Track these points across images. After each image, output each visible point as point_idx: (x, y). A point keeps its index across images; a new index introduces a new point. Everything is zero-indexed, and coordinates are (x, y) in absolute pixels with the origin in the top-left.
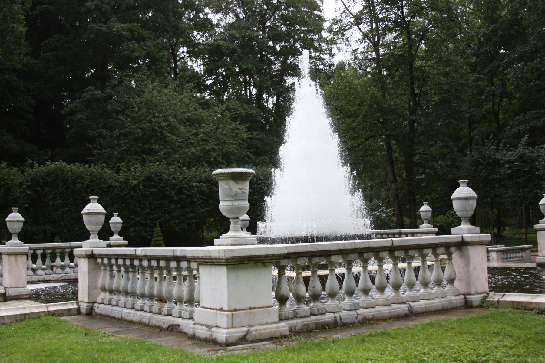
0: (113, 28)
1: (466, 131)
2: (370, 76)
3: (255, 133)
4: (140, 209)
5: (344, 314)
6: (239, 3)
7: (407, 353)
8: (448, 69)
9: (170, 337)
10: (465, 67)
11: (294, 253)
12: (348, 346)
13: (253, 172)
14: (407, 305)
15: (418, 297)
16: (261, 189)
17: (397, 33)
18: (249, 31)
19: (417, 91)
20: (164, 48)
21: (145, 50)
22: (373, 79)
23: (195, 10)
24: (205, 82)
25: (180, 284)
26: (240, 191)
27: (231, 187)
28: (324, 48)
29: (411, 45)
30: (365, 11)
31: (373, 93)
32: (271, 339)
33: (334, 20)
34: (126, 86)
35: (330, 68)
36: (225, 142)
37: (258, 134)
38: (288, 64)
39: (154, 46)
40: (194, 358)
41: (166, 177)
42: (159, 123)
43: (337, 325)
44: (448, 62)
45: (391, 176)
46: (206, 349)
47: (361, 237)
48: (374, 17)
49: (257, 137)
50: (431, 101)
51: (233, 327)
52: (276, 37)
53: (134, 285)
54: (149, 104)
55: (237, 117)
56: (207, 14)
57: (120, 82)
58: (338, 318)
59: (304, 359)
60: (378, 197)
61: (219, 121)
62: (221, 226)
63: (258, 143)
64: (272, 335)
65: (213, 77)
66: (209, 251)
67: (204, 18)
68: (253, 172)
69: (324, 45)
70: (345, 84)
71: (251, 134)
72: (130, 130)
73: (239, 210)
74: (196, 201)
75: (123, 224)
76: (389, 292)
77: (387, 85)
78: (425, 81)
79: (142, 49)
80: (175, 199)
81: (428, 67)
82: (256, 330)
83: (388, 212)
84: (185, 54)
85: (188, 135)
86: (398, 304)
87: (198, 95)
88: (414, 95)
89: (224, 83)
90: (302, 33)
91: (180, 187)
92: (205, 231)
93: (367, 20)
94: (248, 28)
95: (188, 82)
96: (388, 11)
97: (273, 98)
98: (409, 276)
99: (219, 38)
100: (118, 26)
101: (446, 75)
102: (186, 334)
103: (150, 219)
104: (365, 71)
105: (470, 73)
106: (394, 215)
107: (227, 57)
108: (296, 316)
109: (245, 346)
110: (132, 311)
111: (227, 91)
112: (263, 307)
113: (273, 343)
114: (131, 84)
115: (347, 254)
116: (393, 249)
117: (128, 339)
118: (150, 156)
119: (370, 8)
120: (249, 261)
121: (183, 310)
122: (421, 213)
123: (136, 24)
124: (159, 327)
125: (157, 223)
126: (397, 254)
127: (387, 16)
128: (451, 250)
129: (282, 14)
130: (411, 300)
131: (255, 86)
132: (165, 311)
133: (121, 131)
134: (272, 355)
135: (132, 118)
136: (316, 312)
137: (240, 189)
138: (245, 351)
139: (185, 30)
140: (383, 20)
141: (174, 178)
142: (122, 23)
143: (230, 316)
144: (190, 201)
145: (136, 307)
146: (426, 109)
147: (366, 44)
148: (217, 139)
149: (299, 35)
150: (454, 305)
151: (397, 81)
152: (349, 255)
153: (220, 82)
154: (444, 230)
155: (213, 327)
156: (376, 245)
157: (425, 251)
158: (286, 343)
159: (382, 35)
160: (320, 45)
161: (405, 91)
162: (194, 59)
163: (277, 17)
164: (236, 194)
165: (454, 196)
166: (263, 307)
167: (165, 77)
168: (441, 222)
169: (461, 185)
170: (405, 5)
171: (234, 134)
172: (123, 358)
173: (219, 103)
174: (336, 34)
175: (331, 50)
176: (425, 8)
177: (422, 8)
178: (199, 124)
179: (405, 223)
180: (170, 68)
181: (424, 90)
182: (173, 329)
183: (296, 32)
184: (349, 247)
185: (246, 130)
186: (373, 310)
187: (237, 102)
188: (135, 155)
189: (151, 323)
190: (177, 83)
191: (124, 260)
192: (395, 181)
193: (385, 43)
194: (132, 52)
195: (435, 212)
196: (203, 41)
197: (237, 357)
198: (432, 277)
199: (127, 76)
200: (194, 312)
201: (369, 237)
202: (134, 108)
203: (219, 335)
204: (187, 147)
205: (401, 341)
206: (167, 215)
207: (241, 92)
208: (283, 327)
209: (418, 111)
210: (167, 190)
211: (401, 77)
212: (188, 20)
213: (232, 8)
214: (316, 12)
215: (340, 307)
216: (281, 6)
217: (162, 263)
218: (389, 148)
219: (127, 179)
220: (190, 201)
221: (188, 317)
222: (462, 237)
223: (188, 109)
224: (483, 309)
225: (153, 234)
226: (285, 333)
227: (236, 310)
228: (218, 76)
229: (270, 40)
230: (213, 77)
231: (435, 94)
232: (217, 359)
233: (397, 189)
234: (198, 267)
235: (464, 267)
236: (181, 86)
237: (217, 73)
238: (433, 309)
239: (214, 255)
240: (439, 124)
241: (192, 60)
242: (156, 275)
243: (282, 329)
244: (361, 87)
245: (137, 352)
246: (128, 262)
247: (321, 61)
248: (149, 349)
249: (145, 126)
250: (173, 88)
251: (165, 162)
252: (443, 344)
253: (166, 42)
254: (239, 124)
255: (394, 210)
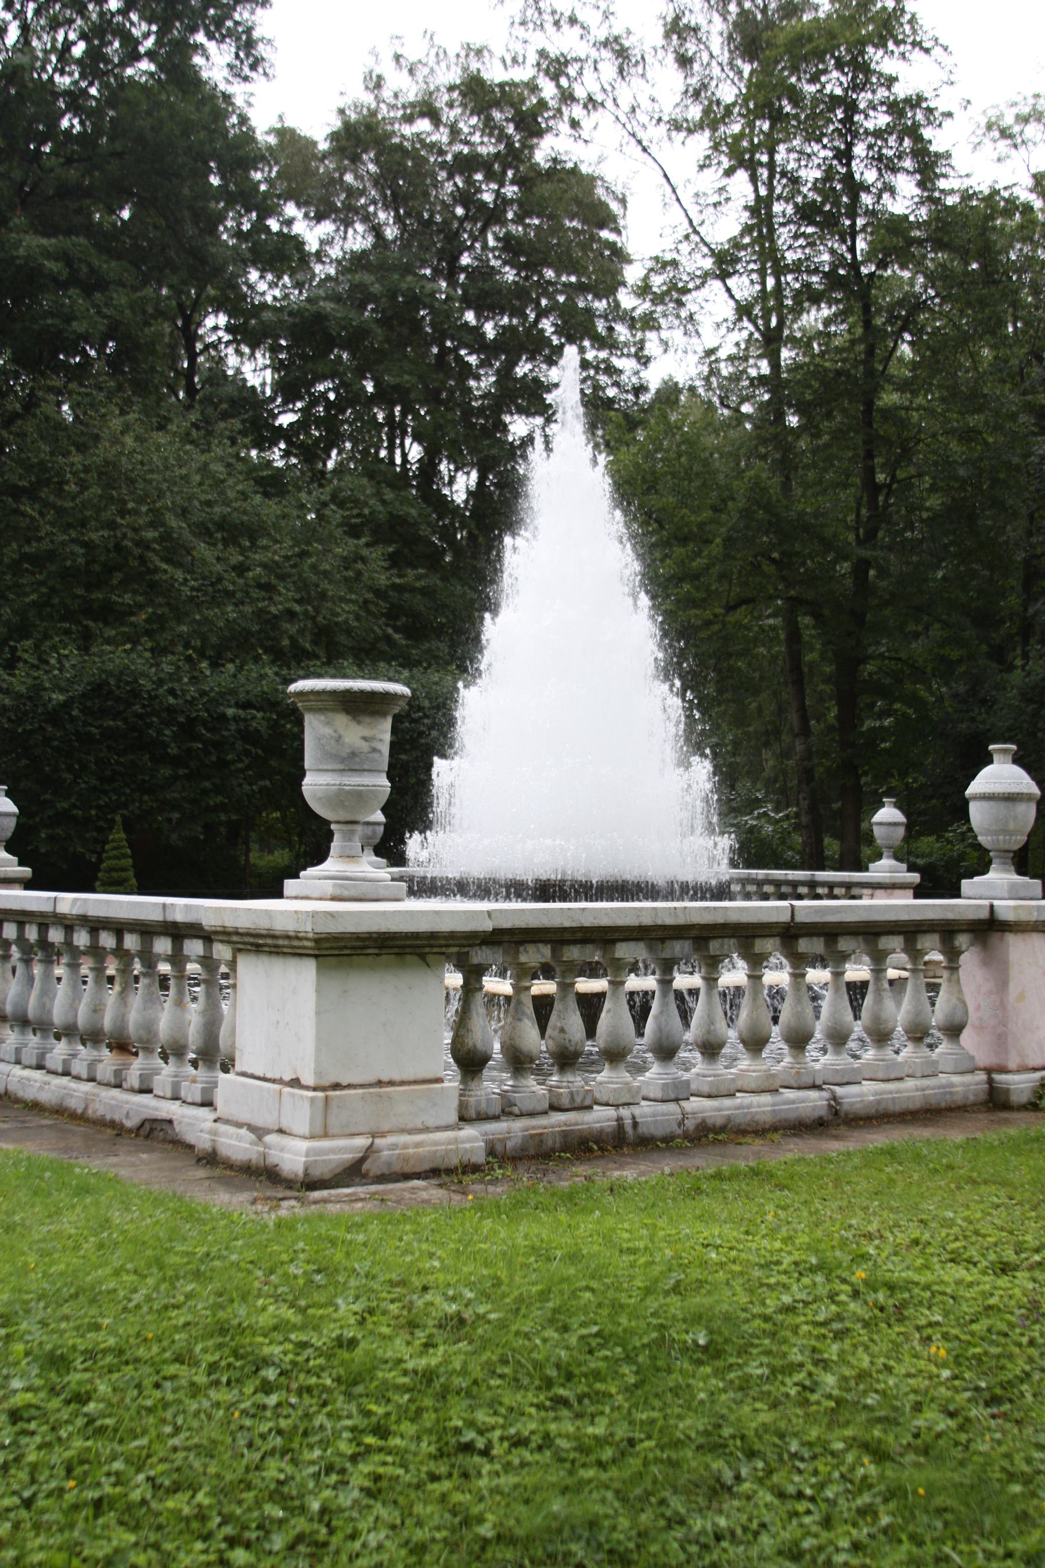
0: (17, 249)
1: (1014, 601)
2: (748, 426)
3: (411, 573)
4: (68, 777)
5: (644, 1110)
6: (385, 196)
7: (819, 1233)
8: (974, 420)
9: (144, 1156)
10: (1023, 418)
11: (511, 931)
12: (653, 1205)
13: (405, 690)
14: (825, 1094)
15: (858, 1071)
16: (421, 734)
17: (834, 309)
18: (409, 278)
19: (880, 477)
20: (161, 314)
21: (105, 317)
22: (758, 437)
23: (257, 208)
24: (275, 417)
25: (179, 1003)
26: (365, 746)
27: (341, 731)
28: (622, 339)
29: (872, 343)
30: (747, 240)
31: (757, 477)
32: (434, 1173)
33: (656, 259)
34: (47, 419)
35: (637, 397)
36: (323, 596)
37: (419, 578)
38: (516, 380)
39: (132, 308)
40: (212, 1219)
41: (149, 686)
42: (135, 530)
43: (624, 1142)
44: (974, 400)
45: (793, 717)
46: (245, 1196)
47: (700, 891)
48: (770, 258)
49: (418, 584)
50: (921, 508)
51: (326, 1135)
52: (487, 296)
53: (46, 999)
54: (109, 474)
55: (363, 524)
56: (289, 222)
57: (30, 403)
58: (628, 1122)
59: (526, 1236)
60: (754, 772)
61: (310, 532)
62: (300, 835)
63: (418, 603)
64: (438, 1163)
65: (299, 405)
66: (268, 913)
67: (280, 233)
68: (405, 690)
69: (622, 332)
70: (678, 445)
71: (400, 576)
72: (51, 546)
73: (360, 797)
74: (233, 762)
75: (18, 817)
76: (778, 1052)
77: (796, 455)
78: (905, 450)
79: (99, 313)
80: (173, 750)
81: (917, 410)
82: (394, 1147)
83: (781, 820)
84: (221, 333)
85: (219, 568)
86: (799, 1088)
87: (254, 453)
88: (872, 488)
89: (330, 424)
90: (561, 292)
91: (188, 717)
92: (255, 846)
93: (752, 266)
94: (408, 269)
95: (225, 416)
96: (811, 245)
97: (468, 474)
98: (832, 1006)
99: (322, 293)
100: (31, 244)
101: (968, 436)
102: (191, 1147)
103: (98, 807)
104: (737, 410)
105: (1035, 434)
106: (797, 827)
107: (342, 348)
108: (507, 1110)
109: (360, 1190)
110: (38, 1075)
111: (338, 446)
112: (415, 1082)
113: (440, 1186)
114: (59, 412)
115: (663, 940)
116: (793, 931)
117: (26, 1154)
118: (106, 623)
119: (760, 232)
120: (380, 948)
121: (186, 1078)
122: (875, 829)
123: (82, 240)
124: (113, 1124)
125: (118, 818)
126: (804, 945)
127: (807, 259)
128: (957, 943)
129: (508, 234)
130: (838, 1080)
131: (417, 438)
132: (133, 1078)
133: (26, 549)
134: (435, 1221)
135: (60, 511)
136: (565, 1102)
137: (365, 739)
138: (359, 1205)
139: (226, 264)
140: (797, 268)
141: (172, 692)
142: (44, 235)
143: (320, 1104)
144: (214, 758)
145: (49, 1064)
146: (904, 530)
147: (745, 334)
148: (303, 585)
149: (551, 297)
150: (959, 1099)
151: (827, 446)
152: (668, 943)
153: (319, 422)
154: (938, 881)
155: (268, 1132)
156: (745, 919)
157: (886, 942)
158: (478, 1187)
159: (792, 310)
160: (611, 329)
161: (848, 477)
162: (246, 350)
163: (491, 243)
164: (353, 754)
165: (974, 787)
166: (415, 1082)
167: (161, 398)
168: (930, 854)
169: (996, 757)
170: (863, 230)
171: (351, 573)
172: (7, 1213)
173: (312, 481)
174: (658, 299)
175: (641, 345)
176: (920, 242)
177: (911, 242)
178: (253, 541)
179: (827, 853)
180: (176, 371)
181: (901, 474)
182: (155, 1133)
183: (545, 288)
184: (669, 921)
185: (385, 564)
186: (727, 1102)
187: (365, 481)
188: (62, 620)
189: (90, 1111)
190: (193, 417)
191: (21, 925)
192: (805, 731)
193: (798, 335)
194: (69, 319)
195: (913, 829)
196: (275, 298)
197: (336, 1221)
198: (899, 1013)
199: (51, 389)
200: (215, 1085)
201: (721, 892)
202: (67, 482)
203: (287, 1156)
204: (214, 602)
205: (804, 1196)
206: (146, 798)
207: (377, 452)
208: (469, 1140)
209: (880, 534)
210: (149, 725)
211: (838, 435)
212: (232, 237)
213: (365, 207)
214: (605, 234)
215: (634, 1091)
216: (505, 211)
217: (131, 942)
218: (794, 636)
219: (37, 688)
220: (214, 758)
221: (198, 1099)
222: (992, 906)
223: (222, 493)
224: (1040, 1115)
225: (103, 851)
226: (474, 1160)
227: (336, 1086)
228: (314, 402)
229: (469, 308)
230: (299, 405)
231: (933, 489)
232: (278, 1225)
233: (808, 755)
234: (235, 958)
235: (991, 992)
236: (205, 425)
237: (311, 395)
238: (897, 1108)
239: (282, 925)
240: (940, 574)
241: (238, 352)
242: (111, 971)
243: (468, 1146)
244: (721, 456)
245: (50, 1194)
246: (32, 934)
247: (610, 376)
248: (83, 1190)
249: (95, 536)
250: (182, 430)
251: (149, 645)
252: (923, 1211)
253: (168, 298)
254: (368, 545)
255: (797, 815)
